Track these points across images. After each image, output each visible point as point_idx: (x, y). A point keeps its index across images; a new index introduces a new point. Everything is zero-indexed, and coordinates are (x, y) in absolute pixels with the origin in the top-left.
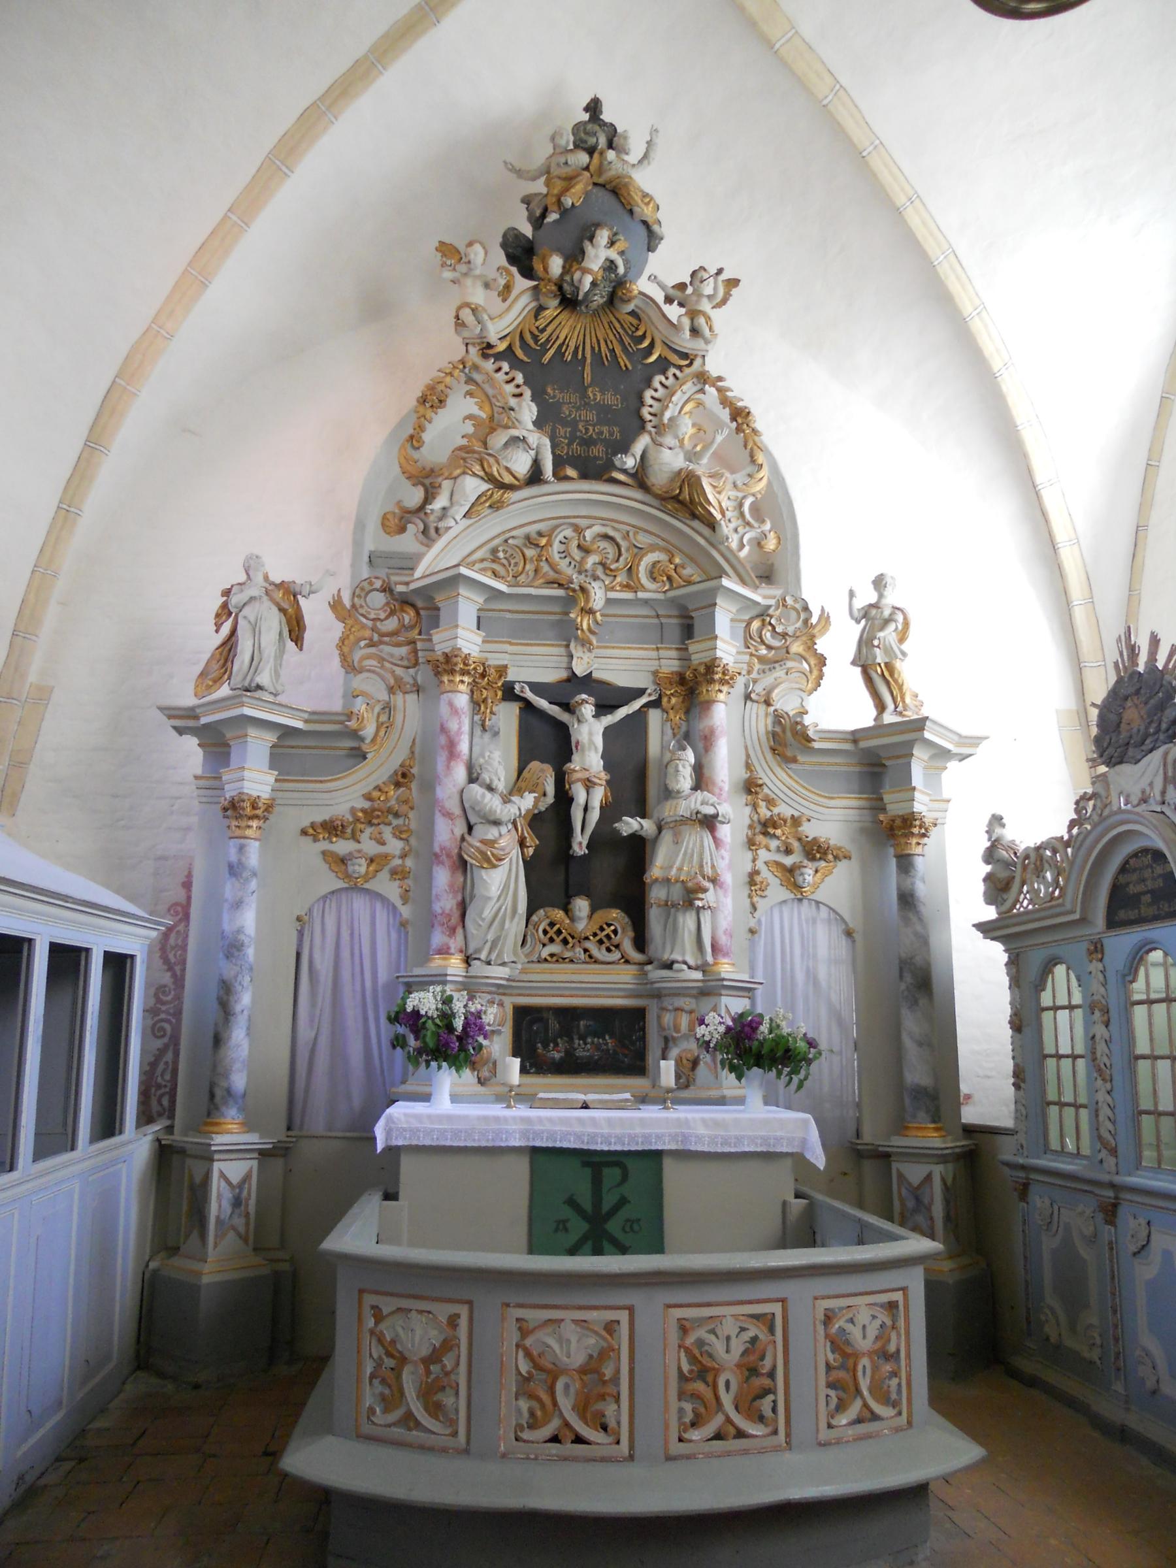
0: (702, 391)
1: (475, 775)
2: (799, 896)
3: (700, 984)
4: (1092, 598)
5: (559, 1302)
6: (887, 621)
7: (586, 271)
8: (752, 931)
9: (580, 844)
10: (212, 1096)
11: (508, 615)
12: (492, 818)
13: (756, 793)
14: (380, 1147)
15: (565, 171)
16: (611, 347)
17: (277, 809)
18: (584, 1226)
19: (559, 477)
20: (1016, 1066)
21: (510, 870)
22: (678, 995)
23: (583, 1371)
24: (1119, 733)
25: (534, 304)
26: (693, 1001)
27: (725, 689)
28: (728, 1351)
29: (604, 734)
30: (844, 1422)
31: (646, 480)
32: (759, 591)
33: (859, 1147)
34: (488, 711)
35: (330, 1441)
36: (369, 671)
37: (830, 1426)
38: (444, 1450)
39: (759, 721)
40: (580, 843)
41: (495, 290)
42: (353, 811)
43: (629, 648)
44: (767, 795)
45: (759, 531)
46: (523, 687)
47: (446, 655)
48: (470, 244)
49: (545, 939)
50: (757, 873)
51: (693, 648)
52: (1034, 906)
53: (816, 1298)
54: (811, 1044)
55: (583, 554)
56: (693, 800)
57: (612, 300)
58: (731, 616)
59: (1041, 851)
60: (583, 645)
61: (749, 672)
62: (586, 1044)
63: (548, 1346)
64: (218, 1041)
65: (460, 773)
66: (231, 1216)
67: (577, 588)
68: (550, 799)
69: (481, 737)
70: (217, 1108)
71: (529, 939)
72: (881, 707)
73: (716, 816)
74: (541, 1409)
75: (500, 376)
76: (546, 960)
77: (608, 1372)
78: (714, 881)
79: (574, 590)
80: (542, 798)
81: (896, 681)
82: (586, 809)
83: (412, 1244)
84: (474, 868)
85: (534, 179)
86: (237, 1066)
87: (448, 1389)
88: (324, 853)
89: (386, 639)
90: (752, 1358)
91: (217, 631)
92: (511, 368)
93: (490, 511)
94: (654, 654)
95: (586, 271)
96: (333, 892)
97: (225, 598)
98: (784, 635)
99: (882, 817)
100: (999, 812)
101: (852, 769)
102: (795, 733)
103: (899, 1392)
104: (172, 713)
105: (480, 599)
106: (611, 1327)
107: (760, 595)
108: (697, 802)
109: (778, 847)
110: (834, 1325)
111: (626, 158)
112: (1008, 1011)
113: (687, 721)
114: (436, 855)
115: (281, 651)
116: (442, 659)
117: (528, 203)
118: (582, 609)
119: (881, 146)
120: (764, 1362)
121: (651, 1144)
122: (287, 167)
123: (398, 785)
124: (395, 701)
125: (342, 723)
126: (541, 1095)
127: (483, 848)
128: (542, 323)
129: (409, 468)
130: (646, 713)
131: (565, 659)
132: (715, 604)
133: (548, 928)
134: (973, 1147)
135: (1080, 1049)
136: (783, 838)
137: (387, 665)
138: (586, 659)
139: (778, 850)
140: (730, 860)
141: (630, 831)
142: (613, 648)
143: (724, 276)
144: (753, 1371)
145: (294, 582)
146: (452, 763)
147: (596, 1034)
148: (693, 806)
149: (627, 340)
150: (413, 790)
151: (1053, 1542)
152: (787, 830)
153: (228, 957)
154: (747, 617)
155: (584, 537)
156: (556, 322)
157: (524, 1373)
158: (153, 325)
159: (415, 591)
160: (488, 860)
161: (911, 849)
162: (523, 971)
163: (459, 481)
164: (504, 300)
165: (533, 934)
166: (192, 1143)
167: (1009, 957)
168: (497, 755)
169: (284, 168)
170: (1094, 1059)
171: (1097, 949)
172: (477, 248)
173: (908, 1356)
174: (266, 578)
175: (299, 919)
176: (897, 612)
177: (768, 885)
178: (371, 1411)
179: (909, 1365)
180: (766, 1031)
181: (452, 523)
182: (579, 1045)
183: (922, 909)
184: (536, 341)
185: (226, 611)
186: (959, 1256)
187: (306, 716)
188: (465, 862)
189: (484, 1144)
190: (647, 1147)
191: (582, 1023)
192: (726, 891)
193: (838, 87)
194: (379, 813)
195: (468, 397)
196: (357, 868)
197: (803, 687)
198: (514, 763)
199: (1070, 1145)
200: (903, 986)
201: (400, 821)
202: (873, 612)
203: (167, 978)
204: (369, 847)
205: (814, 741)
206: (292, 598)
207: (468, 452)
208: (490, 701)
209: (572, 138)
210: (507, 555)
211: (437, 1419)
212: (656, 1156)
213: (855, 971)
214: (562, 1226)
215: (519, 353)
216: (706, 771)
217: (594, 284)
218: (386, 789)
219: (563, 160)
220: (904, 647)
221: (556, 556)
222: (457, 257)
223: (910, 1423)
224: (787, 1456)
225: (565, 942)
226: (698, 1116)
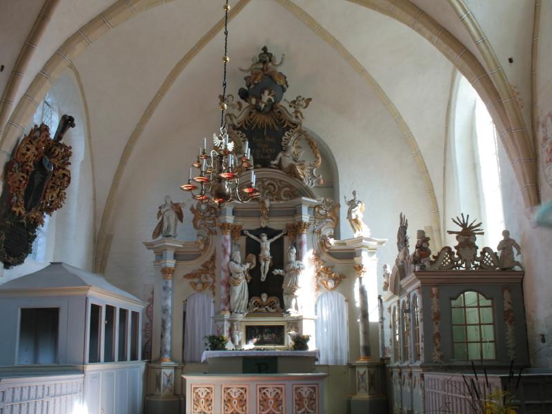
9: (263, 277)
61: (315, 223)
75: (239, 135)
115: (176, 225)
144: (277, 400)
149: (277, 121)
174: (171, 202)
203: (148, 321)
215: (245, 128)
217: (265, 106)
225: (260, 307)
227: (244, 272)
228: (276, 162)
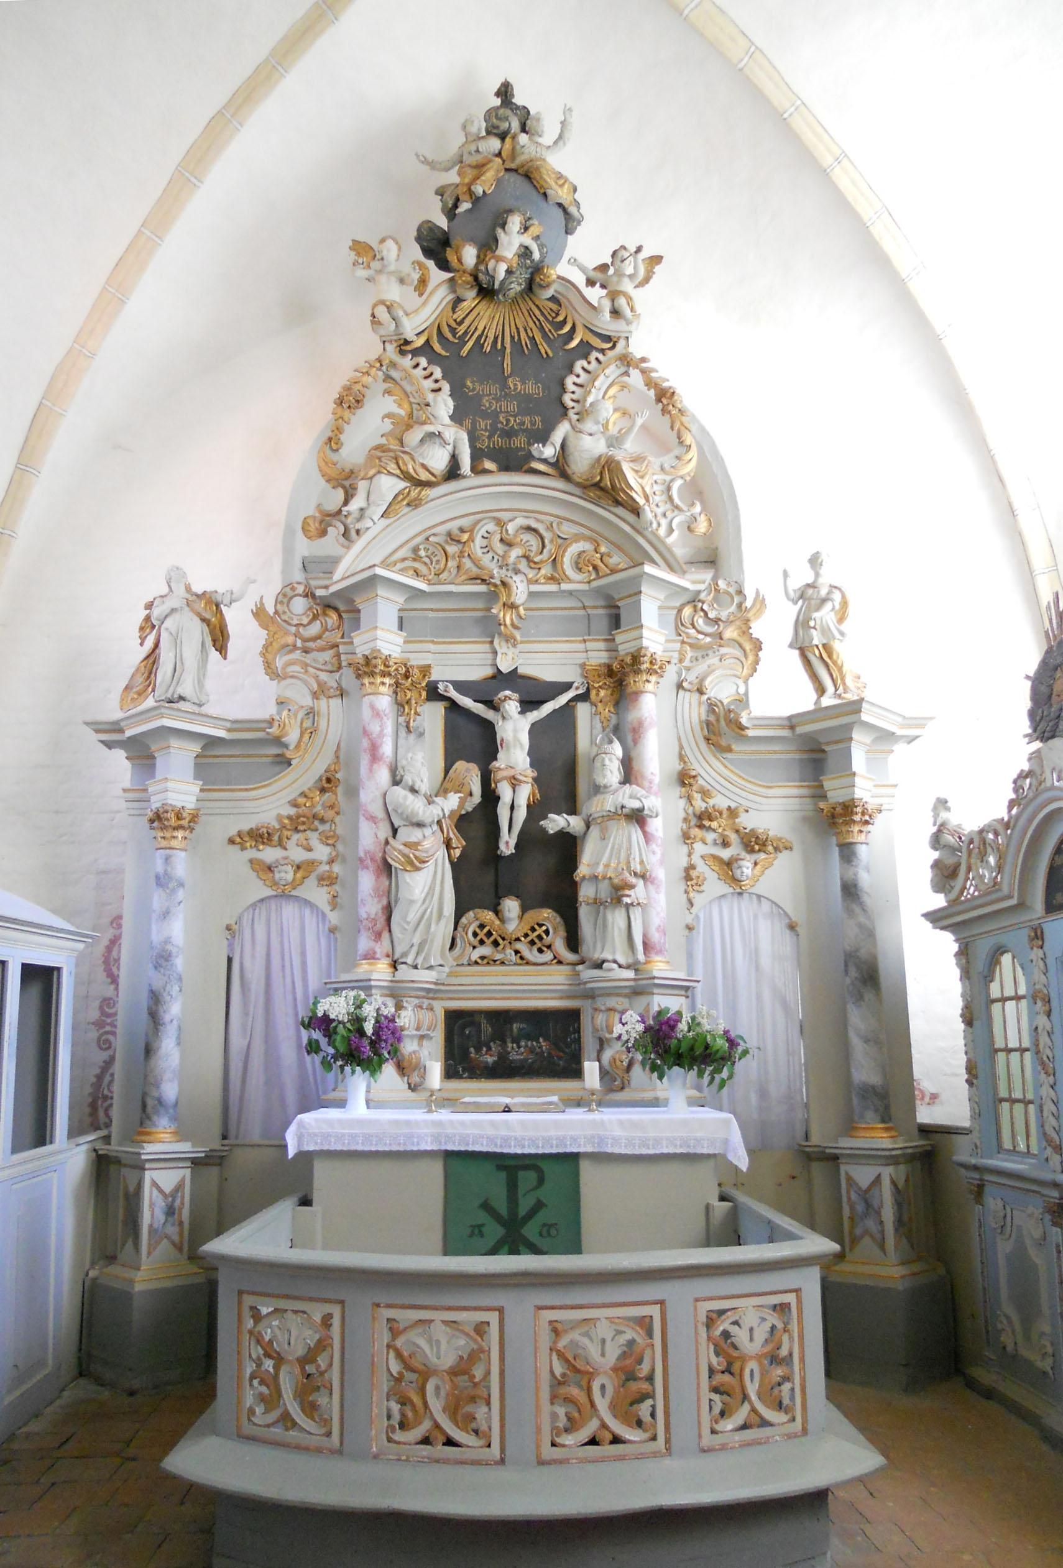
0: (626, 374)
1: (398, 778)
2: (739, 890)
3: (632, 983)
4: (1056, 565)
5: (419, 1302)
6: (824, 601)
7: (500, 259)
8: (690, 928)
9: (507, 844)
10: (144, 1106)
11: (431, 614)
12: (414, 820)
13: (691, 785)
14: (291, 1152)
15: (476, 159)
16: (531, 335)
17: (202, 819)
18: (500, 1231)
19: (477, 470)
20: (969, 1061)
21: (435, 872)
22: (609, 995)
23: (454, 1372)
24: (1051, 706)
25: (451, 297)
26: (626, 1000)
27: (653, 679)
28: (603, 1355)
29: (530, 732)
30: (730, 1427)
31: (566, 468)
32: (687, 576)
33: (807, 1149)
34: (413, 712)
35: (213, 1441)
36: (292, 677)
37: (713, 1432)
38: (319, 1450)
39: (693, 710)
40: (507, 843)
41: (411, 285)
42: (279, 818)
43: (555, 641)
44: (702, 787)
45: (689, 514)
46: (447, 686)
47: (366, 658)
48: (383, 241)
49: (475, 942)
50: (692, 867)
51: (619, 638)
52: (979, 891)
53: (697, 1300)
54: (732, 1043)
55: (507, 548)
56: (621, 794)
57: (530, 287)
58: (659, 603)
59: (984, 834)
60: (507, 641)
61: (681, 661)
62: (519, 1047)
63: (418, 1347)
64: (149, 1051)
65: (383, 775)
66: (164, 1224)
67: (499, 583)
68: (477, 798)
69: (406, 739)
70: (149, 1118)
71: (458, 941)
72: (821, 690)
73: (641, 810)
74: (411, 1411)
75: (419, 372)
76: (476, 963)
77: (478, 1373)
78: (643, 877)
79: (495, 586)
80: (469, 798)
81: (835, 663)
82: (512, 808)
83: (326, 1247)
84: (399, 871)
85: (447, 169)
86: (167, 1076)
87: (322, 1389)
88: (251, 861)
89: (311, 644)
90: (628, 1362)
91: (141, 644)
92: (429, 363)
93: (407, 509)
94: (581, 646)
95: (500, 259)
96: (262, 900)
97: (148, 611)
98: (717, 621)
99: (822, 805)
100: (943, 796)
101: (789, 756)
102: (729, 722)
103: (792, 1398)
104: (99, 728)
105: (400, 599)
106: (481, 1329)
107: (688, 580)
108: (628, 797)
109: (715, 840)
110: (718, 1326)
111: (540, 140)
112: (959, 1004)
113: (617, 714)
114: (361, 860)
116: (362, 661)
117: (442, 195)
118: (504, 604)
119: (803, 107)
120: (642, 1366)
121: (566, 1146)
122: (196, 178)
123: (323, 790)
124: (319, 706)
125: (263, 730)
126: (466, 1100)
127: (406, 850)
128: (459, 315)
129: (328, 471)
130: (574, 707)
131: (490, 656)
132: (640, 592)
133: (478, 930)
134: (929, 1148)
135: (1026, 1043)
136: (720, 830)
137: (311, 670)
138: (510, 655)
139: (715, 843)
140: (663, 855)
141: (557, 829)
142: (540, 642)
143: (644, 254)
145: (216, 592)
146: (375, 766)
147: (529, 1037)
148: (620, 799)
149: (547, 327)
150: (339, 794)
151: (967, 1557)
152: (723, 822)
153: (156, 968)
154: (678, 604)
155: (507, 530)
156: (474, 313)
157: (395, 1374)
158: (75, 345)
159: (333, 594)
160: (412, 863)
161: (853, 837)
162: (450, 975)
163: (375, 480)
164: (421, 295)
165: (462, 936)
166: (127, 1152)
167: (960, 947)
168: (419, 756)
169: (193, 180)
170: (1038, 1052)
171: (1038, 936)
172: (390, 243)
173: (802, 1360)
174: (188, 589)
175: (228, 928)
176: (834, 590)
177: (705, 879)
178: (251, 1412)
179: (803, 1369)
180: (686, 1029)
181: (369, 524)
182: (513, 1048)
183: (865, 899)
184: (454, 334)
185: (150, 624)
186: (914, 1261)
187: (228, 725)
188: (390, 866)
189: (395, 1148)
190: (561, 1150)
191: (515, 1026)
192: (658, 887)
193: (753, 49)
194: (305, 819)
195: (386, 395)
196: (283, 875)
197: (739, 673)
198: (441, 764)
199: (1022, 1147)
200: (848, 981)
201: (326, 827)
202: (810, 591)
204: (297, 854)
205: (747, 728)
206: (215, 608)
207: (384, 452)
208: (413, 702)
209: (484, 125)
210: (430, 552)
211: (313, 1419)
212: (571, 1159)
213: (799, 965)
214: (477, 1230)
215: (437, 347)
216: (635, 765)
217: (509, 272)
218: (311, 795)
219: (473, 148)
220: (844, 627)
221: (479, 552)
222: (371, 254)
223: (805, 1431)
224: (667, 1461)
225: (496, 944)
226: (613, 1117)
227: (439, 823)
228: (549, 451)
